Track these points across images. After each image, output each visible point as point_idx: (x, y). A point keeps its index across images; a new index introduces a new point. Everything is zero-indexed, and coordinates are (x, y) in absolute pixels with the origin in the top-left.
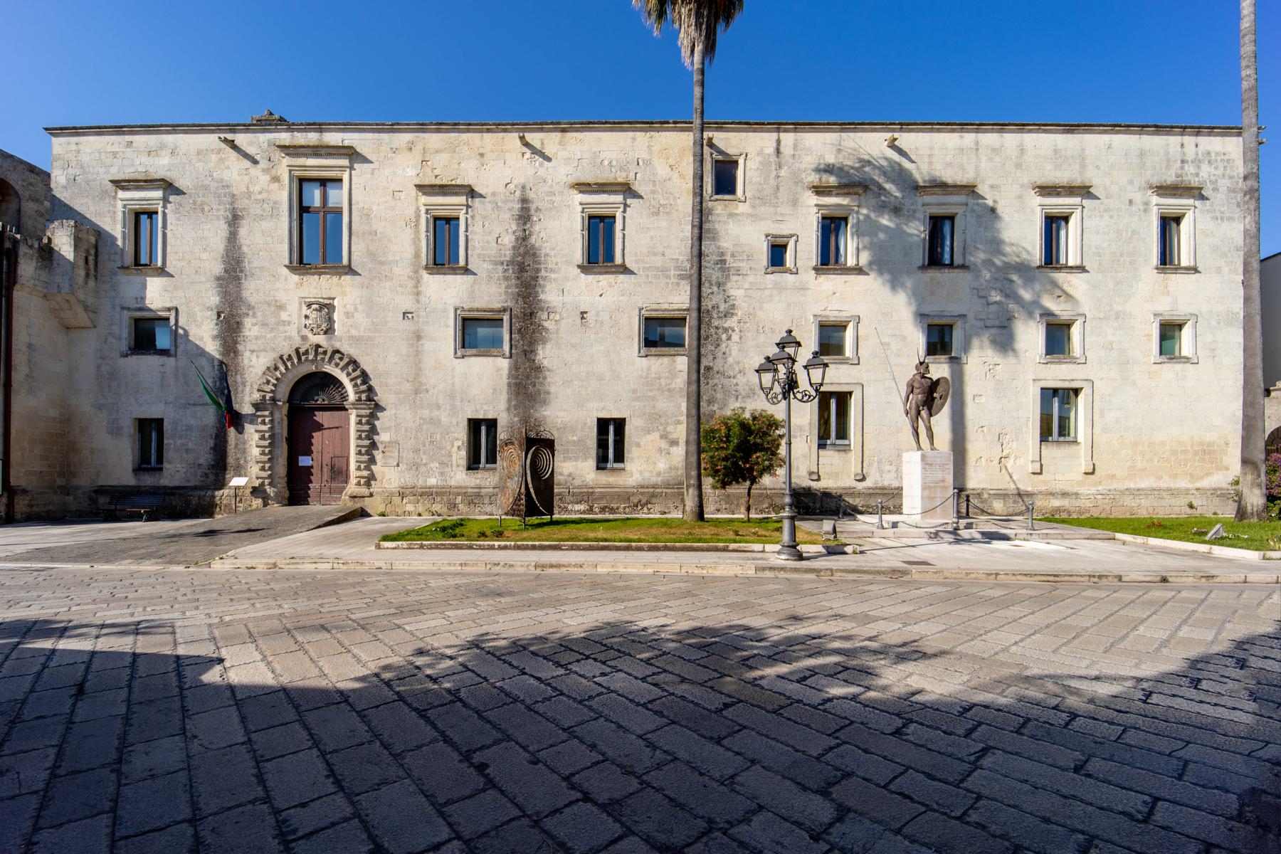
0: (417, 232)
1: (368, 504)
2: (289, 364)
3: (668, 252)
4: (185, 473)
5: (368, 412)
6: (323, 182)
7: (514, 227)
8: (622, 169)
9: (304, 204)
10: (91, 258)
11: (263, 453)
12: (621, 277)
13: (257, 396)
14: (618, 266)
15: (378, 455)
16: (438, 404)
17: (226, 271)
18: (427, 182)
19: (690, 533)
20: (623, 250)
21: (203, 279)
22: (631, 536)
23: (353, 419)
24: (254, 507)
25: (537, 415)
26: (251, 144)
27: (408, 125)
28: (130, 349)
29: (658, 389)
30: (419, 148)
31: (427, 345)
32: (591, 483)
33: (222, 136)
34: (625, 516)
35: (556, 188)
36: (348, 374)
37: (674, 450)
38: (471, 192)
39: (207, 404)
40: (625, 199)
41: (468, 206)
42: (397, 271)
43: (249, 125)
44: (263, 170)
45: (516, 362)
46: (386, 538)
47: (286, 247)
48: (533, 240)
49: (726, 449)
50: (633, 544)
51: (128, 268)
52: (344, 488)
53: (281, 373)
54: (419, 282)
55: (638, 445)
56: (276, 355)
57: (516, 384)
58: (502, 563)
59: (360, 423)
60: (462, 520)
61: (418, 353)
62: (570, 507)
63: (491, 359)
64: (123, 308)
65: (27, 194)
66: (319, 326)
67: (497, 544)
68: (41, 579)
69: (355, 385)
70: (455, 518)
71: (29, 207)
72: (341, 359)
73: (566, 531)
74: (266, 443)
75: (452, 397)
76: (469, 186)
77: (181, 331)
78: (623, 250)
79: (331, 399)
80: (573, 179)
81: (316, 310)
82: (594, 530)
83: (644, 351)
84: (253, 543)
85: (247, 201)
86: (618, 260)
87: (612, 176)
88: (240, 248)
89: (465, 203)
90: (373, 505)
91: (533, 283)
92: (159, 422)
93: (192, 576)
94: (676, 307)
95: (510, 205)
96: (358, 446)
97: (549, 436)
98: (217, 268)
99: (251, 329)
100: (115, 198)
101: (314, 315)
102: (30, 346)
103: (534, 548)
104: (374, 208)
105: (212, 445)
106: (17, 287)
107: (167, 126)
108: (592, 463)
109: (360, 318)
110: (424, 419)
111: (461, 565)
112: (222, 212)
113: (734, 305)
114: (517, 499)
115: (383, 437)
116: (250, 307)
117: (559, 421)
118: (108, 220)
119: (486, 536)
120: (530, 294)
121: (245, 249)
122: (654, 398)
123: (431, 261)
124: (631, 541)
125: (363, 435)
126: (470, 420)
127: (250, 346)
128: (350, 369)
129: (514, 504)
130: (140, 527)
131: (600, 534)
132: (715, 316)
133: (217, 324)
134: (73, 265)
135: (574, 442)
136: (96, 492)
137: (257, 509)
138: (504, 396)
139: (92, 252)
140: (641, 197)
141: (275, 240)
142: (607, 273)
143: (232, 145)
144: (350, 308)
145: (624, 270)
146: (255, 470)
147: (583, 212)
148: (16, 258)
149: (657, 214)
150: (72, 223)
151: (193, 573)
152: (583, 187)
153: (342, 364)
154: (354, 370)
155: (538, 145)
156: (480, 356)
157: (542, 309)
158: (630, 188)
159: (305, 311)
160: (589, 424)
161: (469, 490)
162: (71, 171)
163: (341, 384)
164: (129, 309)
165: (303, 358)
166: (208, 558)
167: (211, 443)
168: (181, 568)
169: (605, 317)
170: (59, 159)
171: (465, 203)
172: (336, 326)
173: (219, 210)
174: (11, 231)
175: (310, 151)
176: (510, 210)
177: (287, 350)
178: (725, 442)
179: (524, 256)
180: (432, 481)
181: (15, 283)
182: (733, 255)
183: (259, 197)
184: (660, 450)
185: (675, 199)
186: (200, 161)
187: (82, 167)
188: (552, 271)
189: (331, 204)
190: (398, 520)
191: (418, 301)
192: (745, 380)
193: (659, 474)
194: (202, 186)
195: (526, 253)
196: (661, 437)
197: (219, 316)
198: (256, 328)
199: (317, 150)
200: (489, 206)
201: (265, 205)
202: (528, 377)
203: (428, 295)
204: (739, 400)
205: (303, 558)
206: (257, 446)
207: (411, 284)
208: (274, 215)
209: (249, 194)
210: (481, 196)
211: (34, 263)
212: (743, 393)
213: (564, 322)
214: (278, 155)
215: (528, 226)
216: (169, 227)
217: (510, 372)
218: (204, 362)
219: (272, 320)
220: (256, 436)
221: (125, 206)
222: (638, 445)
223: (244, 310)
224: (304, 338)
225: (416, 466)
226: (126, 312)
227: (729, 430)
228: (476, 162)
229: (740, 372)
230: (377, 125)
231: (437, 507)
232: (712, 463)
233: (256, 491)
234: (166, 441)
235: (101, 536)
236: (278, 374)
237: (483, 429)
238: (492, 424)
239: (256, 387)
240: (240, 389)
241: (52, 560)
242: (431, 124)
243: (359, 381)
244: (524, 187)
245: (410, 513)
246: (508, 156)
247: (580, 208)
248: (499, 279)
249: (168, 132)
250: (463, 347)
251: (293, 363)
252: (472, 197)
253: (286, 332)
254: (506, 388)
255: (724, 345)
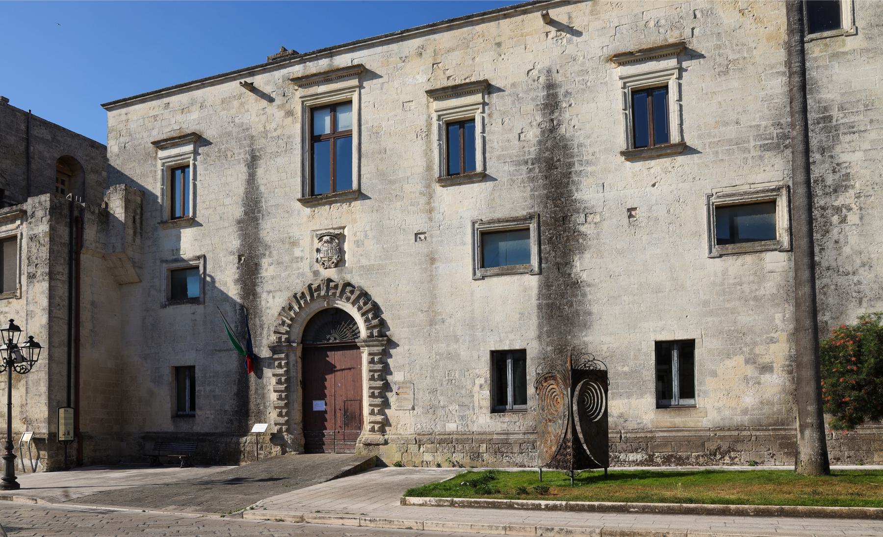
0: (429, 142)
1: (384, 453)
2: (302, 302)
3: (743, 119)
4: (213, 419)
5: (380, 348)
6: (334, 108)
7: (539, 119)
8: (673, 27)
9: (316, 133)
10: (138, 217)
11: (280, 398)
12: (680, 159)
13: (273, 338)
14: (675, 145)
15: (392, 397)
16: (456, 336)
17: (246, 213)
18: (439, 86)
19: (815, 493)
20: (681, 124)
21: (226, 224)
22: (725, 495)
23: (365, 357)
24: (274, 454)
25: (576, 342)
26: (267, 83)
27: (417, 29)
28: (168, 300)
29: (740, 298)
30: (429, 53)
31: (441, 268)
32: (650, 426)
33: (243, 81)
34: (702, 468)
35: (588, 64)
36: (359, 309)
37: (766, 378)
38: (487, 88)
39: (231, 350)
40: (679, 62)
41: (484, 104)
42: (408, 188)
43: (266, 65)
44: (279, 107)
45: (548, 278)
46: (412, 493)
47: (299, 180)
48: (562, 130)
49: (858, 372)
50: (732, 507)
51: (166, 222)
52: (358, 435)
53: (295, 313)
54: (431, 197)
55: (714, 374)
56: (290, 294)
57: (547, 305)
58: (557, 529)
59: (372, 362)
60: (490, 472)
61: (432, 279)
62: (622, 456)
63: (516, 277)
64: (162, 261)
65: (89, 168)
66: (330, 259)
67: (543, 503)
68: (104, 522)
69: (367, 320)
70: (482, 469)
71: (91, 178)
72: (352, 292)
73: (630, 489)
74: (282, 387)
75: (472, 326)
76: (486, 81)
77: (208, 279)
78: (681, 124)
79: (343, 337)
80: (610, 51)
81: (327, 242)
82: (667, 487)
83: (716, 250)
84: (278, 493)
85: (264, 141)
86: (675, 138)
87: (662, 37)
88: (257, 189)
89: (481, 101)
90: (389, 454)
91: (565, 180)
92: (192, 369)
93: (227, 527)
94: (760, 187)
95: (533, 94)
96: (370, 388)
97: (603, 368)
98: (238, 212)
99: (268, 270)
100: (155, 158)
101: (325, 248)
102: (93, 303)
103: (592, 509)
104: (384, 124)
105: (236, 391)
106: (83, 250)
107: (196, 82)
108: (650, 400)
109: (371, 246)
110: (441, 355)
111: (505, 528)
112: (242, 155)
113: (848, 175)
114: (562, 447)
115: (396, 377)
116: (267, 247)
117: (605, 348)
118: (150, 180)
119: (528, 494)
120: (562, 194)
121: (262, 188)
122: (733, 311)
123: (444, 172)
124: (728, 502)
125: (376, 375)
126: (493, 353)
127: (267, 287)
128: (361, 302)
129: (558, 452)
130: (178, 472)
131: (680, 493)
132: (820, 193)
133: (238, 268)
134: (124, 225)
135: (625, 373)
136: (143, 438)
137: (276, 457)
138: (534, 322)
139: (138, 211)
140: (702, 56)
141: (289, 175)
142: (659, 156)
143: (251, 87)
144: (360, 236)
145: (684, 149)
146: (273, 415)
147: (624, 88)
148: (82, 225)
149: (726, 72)
150: (123, 186)
151: (228, 523)
152: (623, 58)
153: (353, 297)
154: (365, 304)
155: (563, 20)
156: (502, 275)
157: (577, 211)
158: (686, 48)
159: (317, 244)
160: (644, 349)
161: (495, 437)
162: (122, 140)
163: (352, 319)
164: (166, 261)
165: (315, 294)
166: (237, 510)
167: (235, 389)
168: (216, 517)
169: (661, 212)
170: (113, 130)
171: (481, 101)
172: (347, 257)
173: (240, 154)
174: (78, 200)
175: (321, 78)
176: (533, 99)
177: (300, 287)
178: (855, 364)
179: (552, 150)
180: (451, 427)
181: (82, 246)
182: (842, 108)
183: (275, 134)
184: (746, 379)
185: (749, 50)
186: (224, 109)
187: (130, 135)
188: (588, 163)
189: (341, 128)
190: (417, 472)
191: (431, 219)
192: (872, 275)
193: (745, 412)
194: (226, 133)
195: (555, 146)
196: (747, 362)
197: (240, 259)
198: (272, 267)
199: (327, 77)
200: (508, 100)
201: (280, 141)
202: (563, 296)
203: (441, 211)
204: (864, 304)
205: (328, 512)
206: (275, 391)
207: (423, 200)
208: (288, 150)
209: (265, 133)
210: (499, 90)
211: (95, 228)
212: (870, 295)
213: (605, 225)
214: (292, 87)
215: (556, 114)
216: (199, 178)
217: (540, 291)
218: (228, 308)
219: (286, 258)
220: (274, 380)
221: (163, 164)
222: (714, 374)
223: (261, 250)
224: (316, 273)
225: (432, 409)
226: (164, 265)
227: (860, 346)
228: (492, 53)
229: (863, 265)
230: (386, 36)
231: (457, 457)
232: (834, 393)
233: (276, 438)
234: (197, 388)
235: (149, 481)
236: (292, 313)
237: (509, 363)
238: (519, 356)
239: (272, 329)
240: (259, 333)
241: (113, 503)
242: (442, 23)
243: (370, 316)
244: (549, 71)
245: (428, 464)
246: (529, 39)
247: (620, 84)
248: (523, 182)
249: (198, 88)
250: (483, 266)
251: (306, 301)
252: (489, 93)
253: (299, 269)
254: (535, 311)
255: (835, 231)
